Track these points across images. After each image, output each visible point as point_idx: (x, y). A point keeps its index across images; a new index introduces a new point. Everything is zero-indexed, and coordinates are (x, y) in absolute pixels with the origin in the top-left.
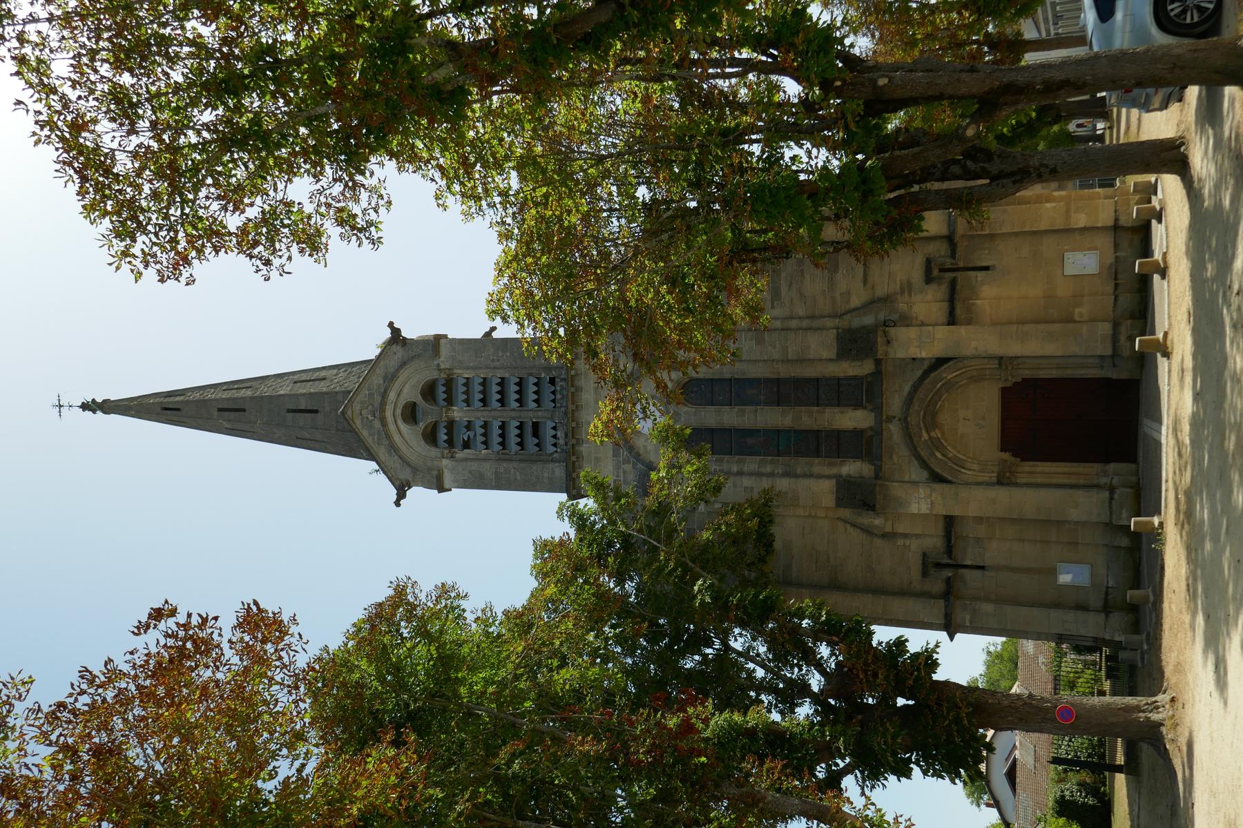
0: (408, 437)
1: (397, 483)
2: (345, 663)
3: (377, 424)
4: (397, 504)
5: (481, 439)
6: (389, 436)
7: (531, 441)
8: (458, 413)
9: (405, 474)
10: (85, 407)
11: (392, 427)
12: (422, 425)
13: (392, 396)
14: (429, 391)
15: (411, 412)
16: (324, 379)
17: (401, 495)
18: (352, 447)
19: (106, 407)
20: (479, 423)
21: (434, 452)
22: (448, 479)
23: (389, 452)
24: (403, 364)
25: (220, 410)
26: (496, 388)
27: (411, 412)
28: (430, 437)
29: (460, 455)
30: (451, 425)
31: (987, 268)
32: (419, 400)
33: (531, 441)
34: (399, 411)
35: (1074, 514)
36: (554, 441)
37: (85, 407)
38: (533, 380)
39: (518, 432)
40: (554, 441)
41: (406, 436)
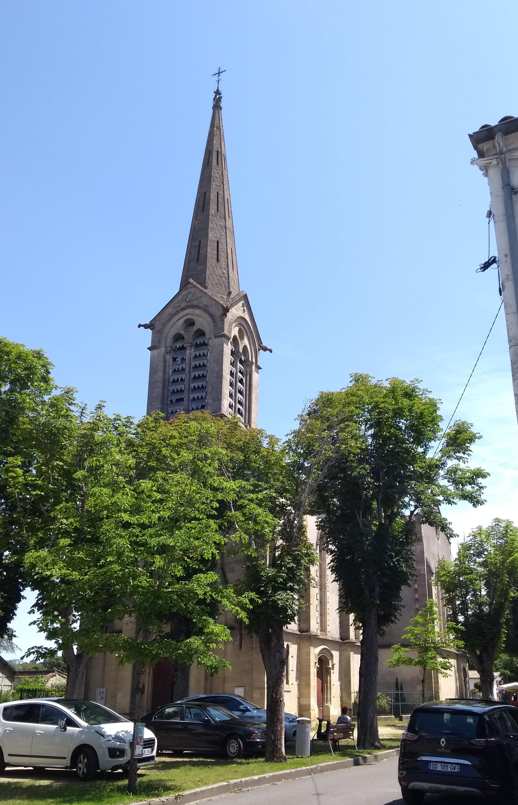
0: (177, 326)
1: (153, 322)
2: (141, 739)
3: (184, 304)
4: (140, 326)
5: (176, 368)
6: (177, 313)
7: (174, 398)
8: (190, 352)
9: (158, 326)
10: (218, 92)
11: (181, 314)
12: (182, 332)
13: (197, 311)
14: (201, 333)
15: (190, 323)
16: (218, 261)
17: (146, 326)
18: (184, 284)
19: (217, 106)
20: (184, 366)
21: (169, 341)
22: (156, 352)
23: (169, 314)
24: (212, 316)
25: (205, 193)
26: (201, 373)
27: (190, 323)
28: (178, 337)
29: (169, 358)
30: (183, 348)
31: (241, 646)
32: (195, 328)
33: (174, 398)
34: (189, 317)
35: (120, 696)
36: (174, 411)
37: (218, 92)
38: (204, 394)
39: (179, 390)
40: (174, 411)
41: (177, 323)
